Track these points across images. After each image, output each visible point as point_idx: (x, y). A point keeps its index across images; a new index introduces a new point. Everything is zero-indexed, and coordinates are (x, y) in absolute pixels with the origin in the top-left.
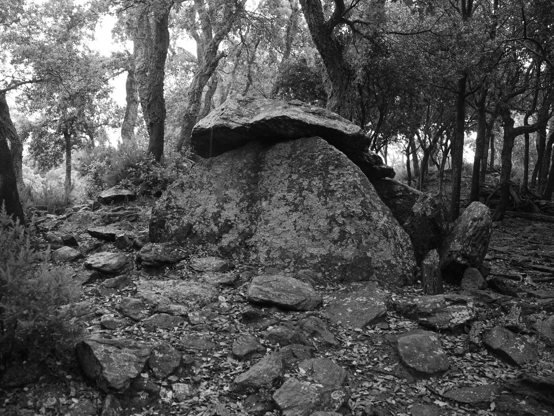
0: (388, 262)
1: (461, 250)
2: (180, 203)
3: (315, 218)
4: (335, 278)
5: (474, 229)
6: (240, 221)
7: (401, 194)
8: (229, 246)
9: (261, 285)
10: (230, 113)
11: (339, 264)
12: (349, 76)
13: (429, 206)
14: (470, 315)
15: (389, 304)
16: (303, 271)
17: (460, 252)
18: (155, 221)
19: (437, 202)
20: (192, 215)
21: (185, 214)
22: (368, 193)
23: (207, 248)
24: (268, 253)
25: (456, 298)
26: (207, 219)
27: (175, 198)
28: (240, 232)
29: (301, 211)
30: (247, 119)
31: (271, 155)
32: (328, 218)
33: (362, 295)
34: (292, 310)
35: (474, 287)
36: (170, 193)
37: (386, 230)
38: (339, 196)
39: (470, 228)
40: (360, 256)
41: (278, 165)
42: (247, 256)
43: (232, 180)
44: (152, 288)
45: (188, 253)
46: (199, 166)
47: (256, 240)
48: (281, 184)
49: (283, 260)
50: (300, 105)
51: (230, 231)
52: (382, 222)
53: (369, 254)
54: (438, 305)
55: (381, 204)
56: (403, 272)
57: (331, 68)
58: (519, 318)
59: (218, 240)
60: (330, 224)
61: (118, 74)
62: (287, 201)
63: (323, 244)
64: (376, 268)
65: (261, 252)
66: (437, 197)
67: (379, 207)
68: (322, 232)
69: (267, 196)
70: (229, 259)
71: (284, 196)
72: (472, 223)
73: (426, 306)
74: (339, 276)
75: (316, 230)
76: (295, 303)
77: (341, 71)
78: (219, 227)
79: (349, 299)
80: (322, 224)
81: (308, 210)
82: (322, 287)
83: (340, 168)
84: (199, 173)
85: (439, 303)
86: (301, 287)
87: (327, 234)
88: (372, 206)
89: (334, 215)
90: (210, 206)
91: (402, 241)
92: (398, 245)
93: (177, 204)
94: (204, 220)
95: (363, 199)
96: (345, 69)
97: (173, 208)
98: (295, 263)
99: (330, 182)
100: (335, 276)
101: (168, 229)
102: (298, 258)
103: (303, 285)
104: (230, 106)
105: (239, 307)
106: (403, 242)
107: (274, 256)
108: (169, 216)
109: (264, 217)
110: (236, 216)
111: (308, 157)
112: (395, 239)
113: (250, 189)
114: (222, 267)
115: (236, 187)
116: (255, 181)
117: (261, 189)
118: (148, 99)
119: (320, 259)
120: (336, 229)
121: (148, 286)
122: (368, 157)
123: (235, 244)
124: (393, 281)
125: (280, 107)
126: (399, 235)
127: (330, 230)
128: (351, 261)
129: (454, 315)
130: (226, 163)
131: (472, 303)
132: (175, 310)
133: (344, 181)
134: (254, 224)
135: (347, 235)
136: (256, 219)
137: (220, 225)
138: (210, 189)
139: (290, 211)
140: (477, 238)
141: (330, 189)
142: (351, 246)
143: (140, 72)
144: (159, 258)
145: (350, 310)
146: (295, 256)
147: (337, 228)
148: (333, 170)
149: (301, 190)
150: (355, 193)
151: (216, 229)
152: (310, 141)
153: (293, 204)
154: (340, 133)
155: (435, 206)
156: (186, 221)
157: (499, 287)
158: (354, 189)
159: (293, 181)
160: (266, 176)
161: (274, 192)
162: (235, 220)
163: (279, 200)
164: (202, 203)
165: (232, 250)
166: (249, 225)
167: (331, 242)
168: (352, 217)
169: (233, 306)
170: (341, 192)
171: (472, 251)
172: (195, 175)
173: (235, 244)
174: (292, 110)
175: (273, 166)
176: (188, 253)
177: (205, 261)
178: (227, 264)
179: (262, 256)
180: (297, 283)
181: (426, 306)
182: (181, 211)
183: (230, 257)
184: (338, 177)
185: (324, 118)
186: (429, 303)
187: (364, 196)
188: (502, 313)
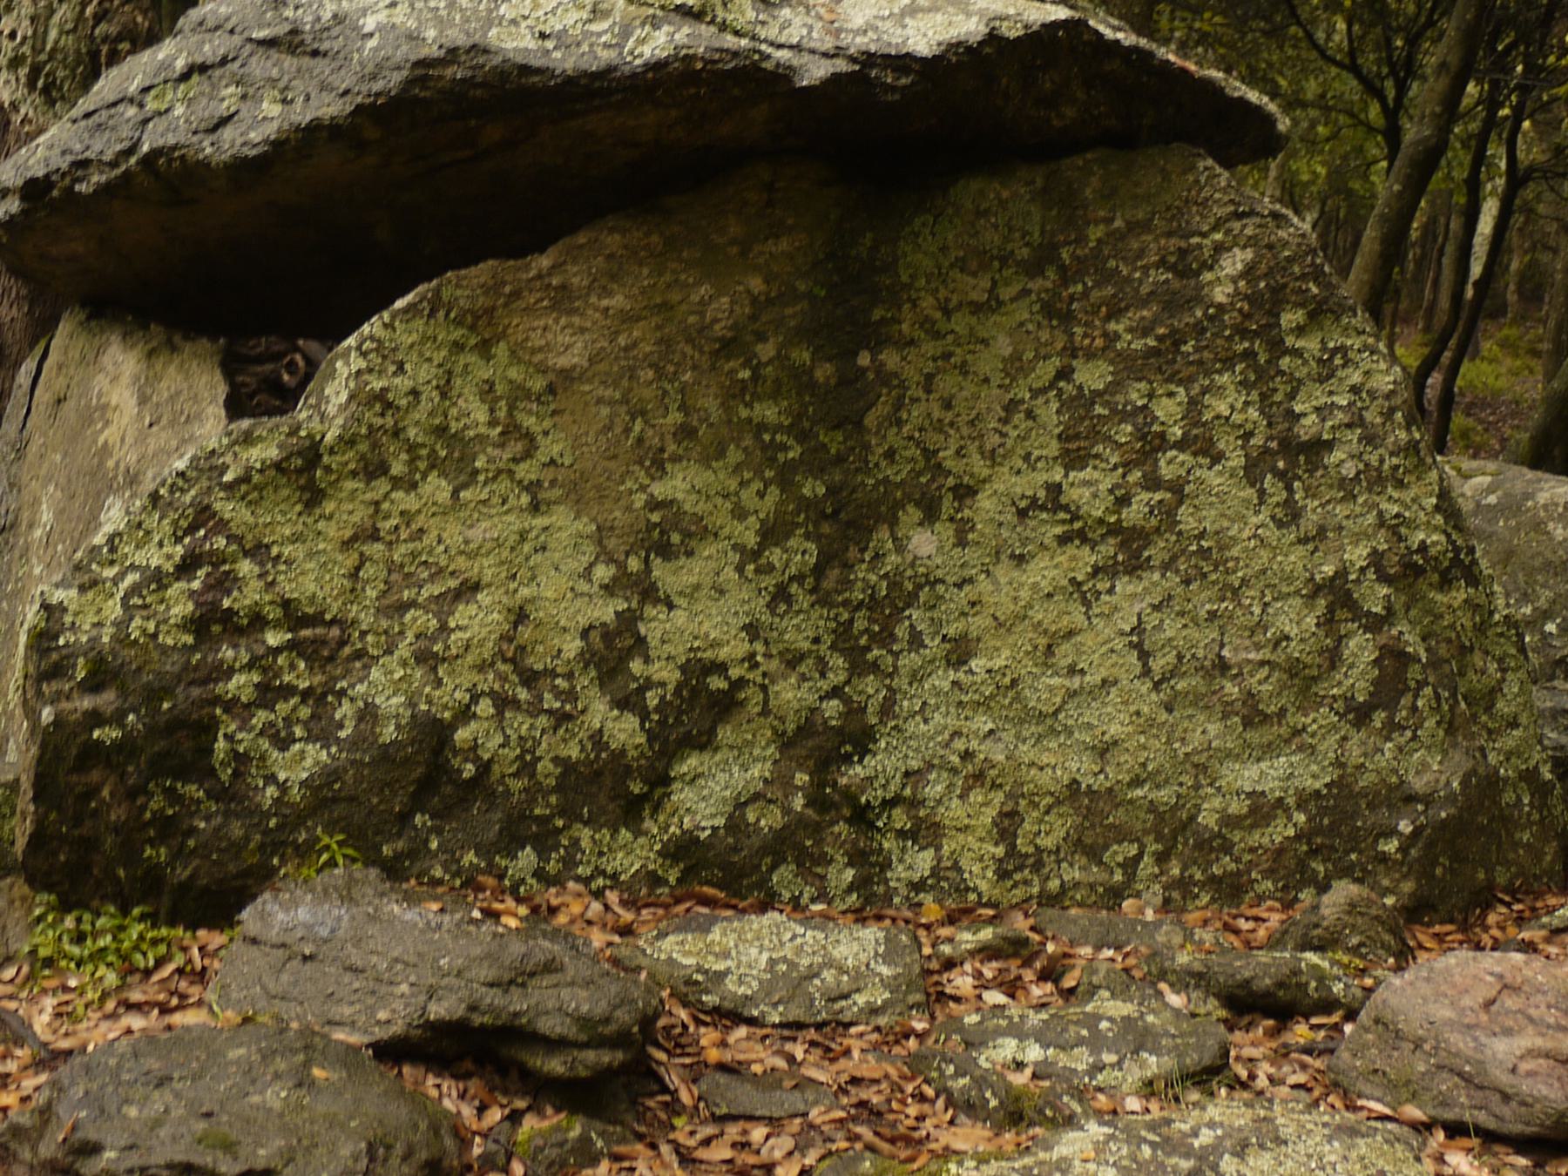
8: (735, 824)
11: (1405, 827)
20: (426, 658)
23: (569, 863)
24: (1006, 826)
27: (258, 551)
31: (922, 250)
38: (1349, 470)
41: (977, 308)
43: (683, 407)
47: (914, 764)
48: (1018, 417)
49: (1094, 854)
51: (725, 733)
59: (643, 798)
60: (1328, 622)
62: (1075, 517)
68: (1293, 669)
69: (940, 496)
71: (1055, 489)
74: (1408, 886)
75: (1262, 663)
78: (644, 716)
80: (1293, 631)
81: (1206, 560)
87: (1315, 679)
89: (1342, 573)
90: (550, 587)
93: (287, 588)
94: (530, 678)
97: (258, 621)
98: (1162, 858)
99: (1292, 396)
107: (1047, 842)
108: (241, 684)
109: (936, 624)
110: (752, 630)
111: (1162, 263)
115: (721, 454)
116: (841, 407)
117: (890, 455)
119: (1301, 818)
123: (787, 811)
127: (1333, 657)
128: (1451, 798)
130: (617, 301)
133: (1355, 390)
134: (875, 667)
136: (885, 638)
137: (652, 698)
139: (1096, 571)
146: (1160, 817)
148: (1300, 331)
149: (1151, 444)
151: (625, 731)
153: (1115, 530)
159: (1082, 402)
161: (980, 467)
164: (487, 568)
165: (764, 850)
167: (1342, 716)
168: (1419, 571)
170: (1355, 447)
173: (787, 811)
175: (947, 313)
182: (323, 641)
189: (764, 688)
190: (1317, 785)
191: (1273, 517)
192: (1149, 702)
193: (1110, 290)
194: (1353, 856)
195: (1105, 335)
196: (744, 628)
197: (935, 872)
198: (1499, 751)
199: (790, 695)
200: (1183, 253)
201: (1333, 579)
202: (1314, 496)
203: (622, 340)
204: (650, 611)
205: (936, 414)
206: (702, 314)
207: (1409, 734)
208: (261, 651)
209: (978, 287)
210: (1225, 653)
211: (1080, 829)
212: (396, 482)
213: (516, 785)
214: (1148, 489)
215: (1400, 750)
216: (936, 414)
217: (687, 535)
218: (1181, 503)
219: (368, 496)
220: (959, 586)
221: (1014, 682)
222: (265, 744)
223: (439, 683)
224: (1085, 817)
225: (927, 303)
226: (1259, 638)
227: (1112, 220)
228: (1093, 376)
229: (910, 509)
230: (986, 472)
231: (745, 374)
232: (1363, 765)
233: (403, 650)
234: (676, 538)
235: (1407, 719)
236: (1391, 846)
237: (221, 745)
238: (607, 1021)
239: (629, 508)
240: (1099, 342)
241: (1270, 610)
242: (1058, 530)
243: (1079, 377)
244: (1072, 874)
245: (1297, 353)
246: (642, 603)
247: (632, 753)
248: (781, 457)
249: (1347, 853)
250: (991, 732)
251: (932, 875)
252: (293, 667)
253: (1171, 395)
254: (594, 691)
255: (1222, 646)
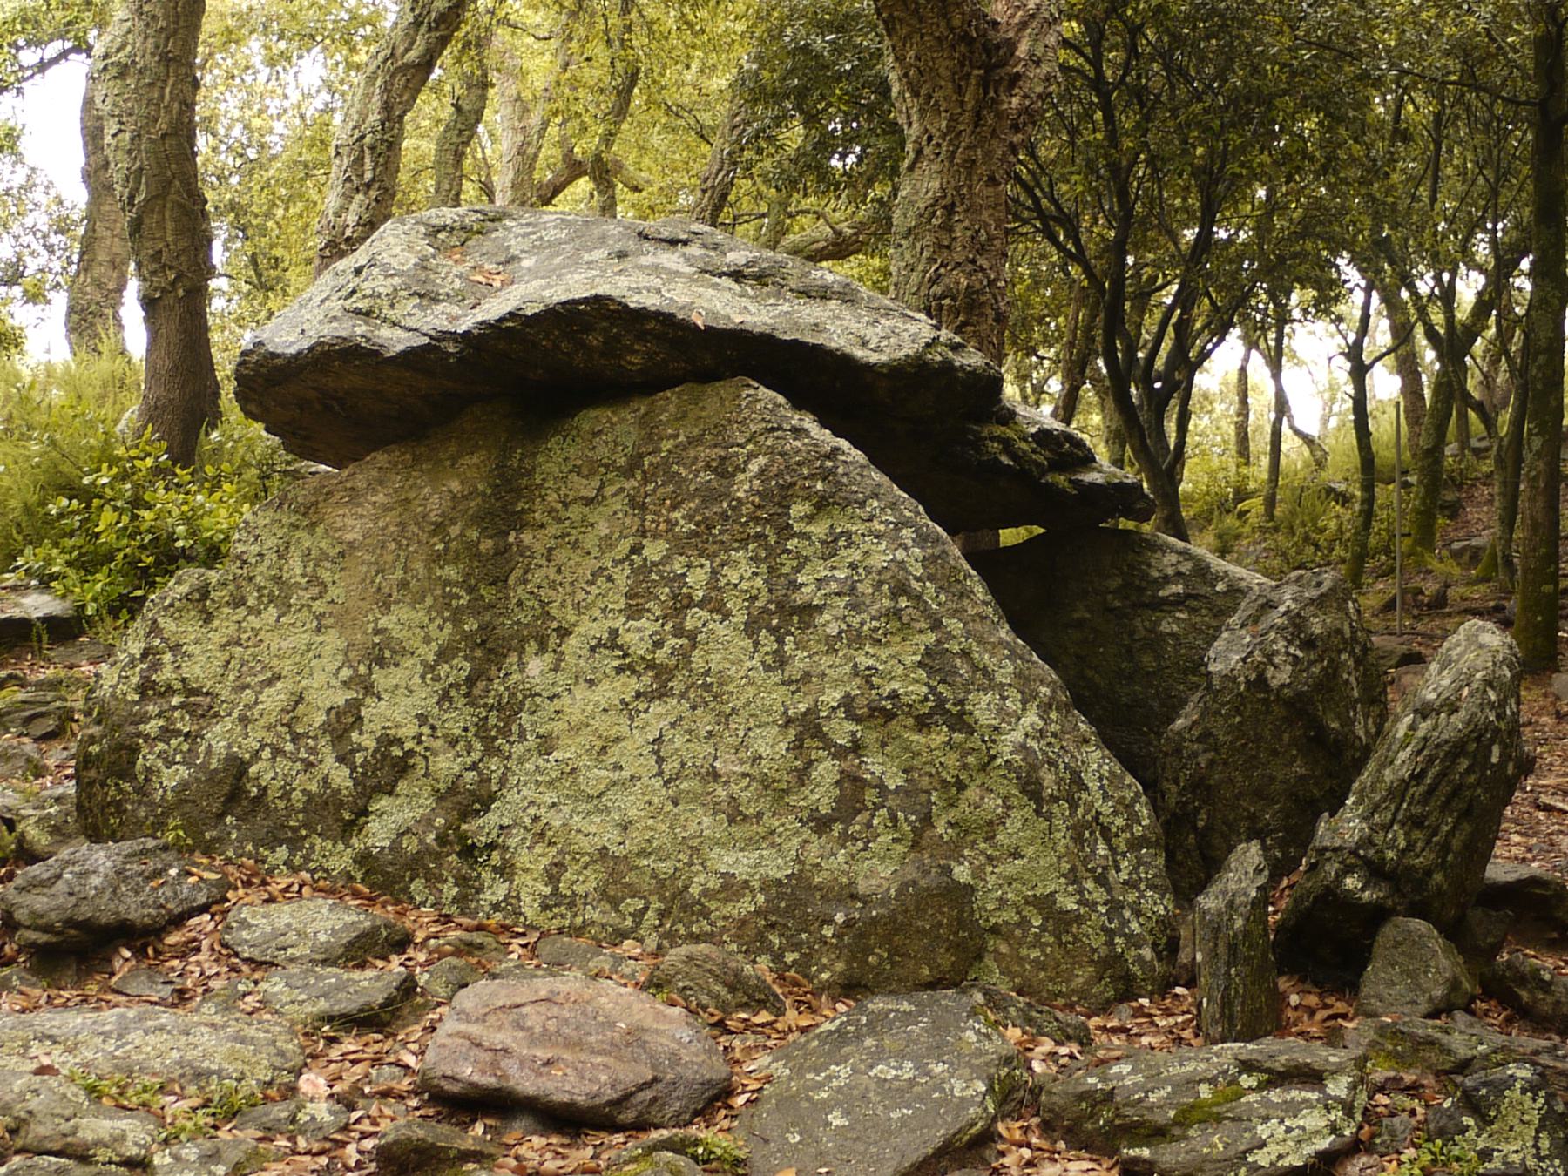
0: (1045, 904)
1: (1359, 846)
2: (197, 670)
3: (738, 723)
4: (825, 976)
5: (1419, 752)
6: (439, 743)
7: (1180, 588)
8: (395, 847)
9: (482, 1019)
10: (384, 286)
11: (839, 918)
12: (989, 69)
13: (1280, 645)
14: (1334, 1128)
15: (1013, 1089)
16: (685, 949)
17: (1354, 852)
18: (95, 749)
19: (1316, 626)
20: (244, 720)
21: (216, 715)
22: (956, 613)
23: (307, 859)
24: (553, 874)
25: (1283, 1059)
26: (306, 736)
27: (176, 648)
28: (442, 786)
29: (683, 695)
30: (455, 310)
31: (555, 462)
32: (789, 722)
33: (902, 1055)
34: (599, 1127)
35: (1414, 1002)
36: (155, 629)
37: (1034, 768)
38: (833, 629)
39: (1403, 747)
40: (923, 883)
41: (588, 502)
42: (469, 889)
44: (26, 1047)
45: (226, 885)
46: (270, 512)
47: (506, 821)
49: (615, 903)
50: (685, 243)
51: (402, 786)
52: (1017, 736)
53: (962, 873)
54: (1205, 1091)
55: (1013, 655)
56: (1110, 944)
57: (909, 36)
58: (1537, 1138)
59: (352, 823)
60: (798, 746)
61: (42, 67)
62: (626, 655)
63: (772, 833)
64: (995, 930)
65: (526, 871)
66: (1320, 602)
67: (1005, 673)
68: (766, 782)
69: (547, 634)
70: (398, 902)
71: (614, 633)
72: (1413, 727)
73: (1153, 1098)
74: (840, 966)
75: (745, 775)
76: (610, 1094)
77: (953, 47)
78: (353, 770)
79: (844, 1071)
80: (765, 751)
81: (710, 690)
82: (764, 1017)
83: (836, 511)
84: (271, 542)
85: (1212, 1081)
86: (649, 1023)
87: (786, 792)
88: (975, 668)
90: (319, 679)
91: (1106, 809)
92: (1087, 828)
94: (296, 738)
95: (931, 638)
96: (970, 42)
97: (170, 691)
98: (662, 915)
99: (798, 570)
100: (823, 968)
101: (147, 780)
102: (674, 897)
103: (659, 1016)
104: (385, 258)
105: (382, 1115)
106: (1115, 813)
108: (152, 727)
110: (422, 719)
111: (708, 467)
112: (1074, 805)
113: (477, 607)
114: (350, 945)
115: (423, 600)
116: (496, 569)
117: (520, 604)
118: (131, 197)
119: (761, 898)
120: (826, 770)
121: (13, 1040)
122: (1007, 445)
124: (1068, 981)
125: (599, 254)
126: (1094, 785)
127: (802, 776)
128: (884, 902)
129: (1263, 1131)
130: (380, 498)
131: (1345, 1080)
132: (98, 1143)
135: (871, 796)
136: (505, 732)
137: (359, 758)
138: (319, 606)
139: (638, 695)
140: (1431, 790)
141: (799, 598)
142: (886, 839)
143: (114, 71)
144: (85, 912)
145: (837, 1119)
146: (661, 884)
147: (828, 764)
148: (810, 519)
149: (681, 605)
150: (896, 613)
151: (341, 778)
152: (716, 399)
153: (651, 665)
154: (842, 363)
155: (1309, 644)
156: (220, 746)
157: (1525, 995)
158: (894, 596)
159: (647, 568)
160: (539, 548)
162: (418, 738)
163: (593, 649)
164: (286, 667)
166: (475, 756)
168: (890, 716)
169: (355, 1115)
170: (840, 612)
171: (1411, 844)
172: (255, 549)
173: (421, 842)
174: (641, 268)
175: (566, 505)
176: (226, 885)
177: (286, 919)
178: (375, 930)
179: (531, 889)
180: (637, 1006)
181: (1153, 1098)
183: (402, 898)
184: (830, 547)
185: (778, 295)
186: (1167, 1081)
187: (937, 625)
188: (1468, 1120)
189: (426, 758)
190: (779, 875)
191: (763, 663)
192: (660, 795)
193: (671, 488)
194: (804, 936)
195: (668, 521)
196: (417, 716)
197: (507, 897)
198: (999, 876)
199: (443, 765)
200: (722, 459)
201: (804, 714)
202: (804, 649)
203: (380, 524)
204: (368, 700)
205: (552, 577)
206: (425, 506)
207: (860, 844)
208: (166, 707)
209: (588, 488)
210: (717, 764)
211: (606, 883)
212: (251, 610)
213: (281, 805)
214: (675, 636)
215: (853, 857)
216: (552, 577)
217: (394, 652)
218: (694, 647)
219: (235, 618)
220: (550, 699)
221: (573, 770)
222: (160, 763)
223: (247, 736)
224: (611, 875)
225: (552, 497)
226: (742, 755)
227: (677, 436)
228: (654, 550)
229: (532, 643)
230: (574, 619)
231: (440, 547)
232: (818, 865)
233: (235, 715)
234: (387, 654)
235: (859, 832)
236: (828, 932)
237: (140, 761)
238: (41, 916)
239: (365, 633)
240: (663, 526)
241: (751, 734)
242: (616, 663)
243: (645, 552)
244: (592, 914)
245: (806, 536)
246: (365, 695)
247: (345, 792)
248: (455, 603)
249: (800, 932)
250: (554, 805)
251: (504, 900)
252: (182, 718)
253: (702, 566)
254: (329, 749)
255: (716, 759)
